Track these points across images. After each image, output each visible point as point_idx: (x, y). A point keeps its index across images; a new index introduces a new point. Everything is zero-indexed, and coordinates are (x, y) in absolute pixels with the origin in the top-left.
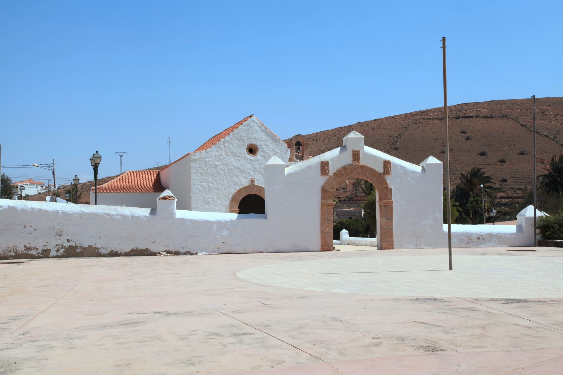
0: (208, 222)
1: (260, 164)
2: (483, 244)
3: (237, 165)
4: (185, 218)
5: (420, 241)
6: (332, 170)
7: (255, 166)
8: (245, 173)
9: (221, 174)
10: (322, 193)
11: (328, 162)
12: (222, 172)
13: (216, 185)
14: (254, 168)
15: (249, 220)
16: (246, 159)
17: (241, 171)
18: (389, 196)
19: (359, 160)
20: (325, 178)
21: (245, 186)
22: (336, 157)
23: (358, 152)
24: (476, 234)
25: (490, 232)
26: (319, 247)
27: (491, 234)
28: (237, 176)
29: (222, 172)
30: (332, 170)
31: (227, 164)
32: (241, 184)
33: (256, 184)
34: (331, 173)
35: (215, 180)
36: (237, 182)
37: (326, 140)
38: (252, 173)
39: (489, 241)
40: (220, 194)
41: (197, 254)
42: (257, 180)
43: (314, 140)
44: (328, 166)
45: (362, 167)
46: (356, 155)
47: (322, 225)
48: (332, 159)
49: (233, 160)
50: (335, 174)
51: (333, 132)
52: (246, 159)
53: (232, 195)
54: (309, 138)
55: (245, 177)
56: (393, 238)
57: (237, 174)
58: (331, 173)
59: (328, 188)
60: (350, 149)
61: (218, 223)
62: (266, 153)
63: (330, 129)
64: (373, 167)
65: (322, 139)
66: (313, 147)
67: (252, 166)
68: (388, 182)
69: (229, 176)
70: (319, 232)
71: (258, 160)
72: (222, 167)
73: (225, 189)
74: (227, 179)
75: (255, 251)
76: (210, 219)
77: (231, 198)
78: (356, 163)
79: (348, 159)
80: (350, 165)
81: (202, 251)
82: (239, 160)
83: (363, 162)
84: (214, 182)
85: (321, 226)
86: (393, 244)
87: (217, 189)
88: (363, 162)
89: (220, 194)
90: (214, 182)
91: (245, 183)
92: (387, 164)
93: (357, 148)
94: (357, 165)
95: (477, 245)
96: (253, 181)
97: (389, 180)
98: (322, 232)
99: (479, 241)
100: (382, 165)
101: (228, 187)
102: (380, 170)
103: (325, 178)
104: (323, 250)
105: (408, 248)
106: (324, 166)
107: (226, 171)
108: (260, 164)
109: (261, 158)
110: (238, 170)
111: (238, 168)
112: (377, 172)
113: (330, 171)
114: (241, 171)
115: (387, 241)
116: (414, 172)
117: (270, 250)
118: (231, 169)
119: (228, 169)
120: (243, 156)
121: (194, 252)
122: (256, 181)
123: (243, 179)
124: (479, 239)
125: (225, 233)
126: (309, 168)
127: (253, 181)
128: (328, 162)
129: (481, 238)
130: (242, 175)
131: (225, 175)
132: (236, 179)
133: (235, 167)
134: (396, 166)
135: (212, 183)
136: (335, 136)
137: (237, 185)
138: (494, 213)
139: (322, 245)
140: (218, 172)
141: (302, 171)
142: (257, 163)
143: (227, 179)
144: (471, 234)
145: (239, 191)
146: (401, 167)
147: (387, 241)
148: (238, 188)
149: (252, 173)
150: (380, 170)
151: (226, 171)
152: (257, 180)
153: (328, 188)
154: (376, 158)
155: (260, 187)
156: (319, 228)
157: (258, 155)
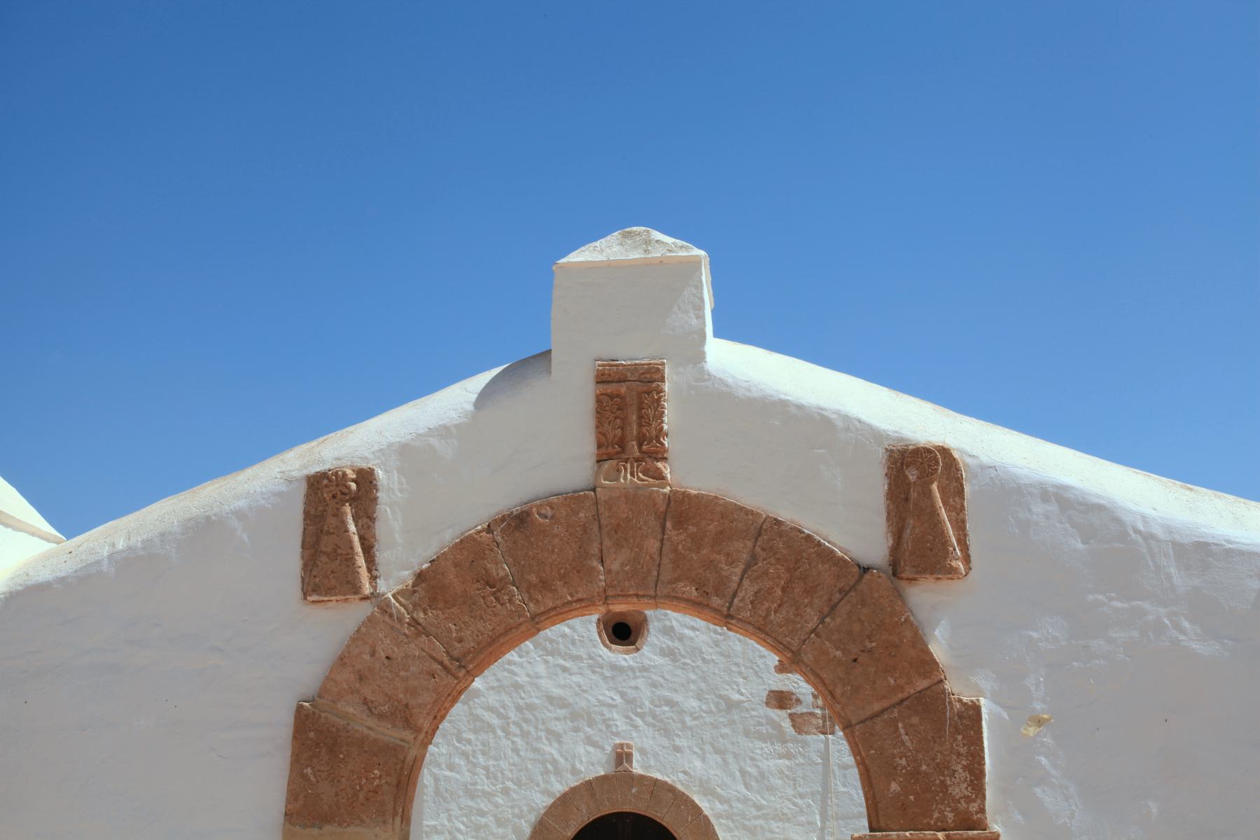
1: (654, 685)
3: (557, 692)
6: (403, 548)
7: (632, 694)
8: (591, 723)
9: (491, 728)
10: (297, 761)
11: (366, 478)
12: (495, 721)
13: (467, 777)
14: (630, 702)
16: (596, 666)
17: (575, 716)
18: (959, 790)
19: (660, 454)
20: (337, 622)
21: (590, 776)
28: (556, 737)
29: (495, 721)
30: (403, 548)
31: (517, 687)
32: (575, 771)
33: (637, 768)
35: (465, 755)
36: (554, 762)
38: (621, 724)
40: (482, 813)
42: (643, 752)
45: (684, 510)
46: (628, 408)
48: (408, 453)
49: (541, 669)
50: (428, 584)
52: (596, 666)
53: (533, 818)
55: (589, 741)
57: (558, 727)
58: (394, 572)
59: (350, 708)
60: (582, 347)
62: (681, 638)
64: (786, 515)
67: (623, 695)
68: (939, 649)
69: (525, 735)
71: (644, 669)
72: (492, 699)
73: (506, 791)
74: (516, 750)
78: (628, 479)
79: (555, 448)
80: (573, 499)
82: (565, 669)
84: (458, 760)
87: (471, 795)
88: (690, 467)
89: (482, 813)
90: (458, 760)
91: (592, 763)
92: (918, 476)
94: (632, 498)
96: (622, 756)
97: (951, 627)
100: (874, 488)
101: (518, 783)
102: (854, 527)
103: (337, 622)
106: (336, 511)
107: (513, 715)
108: (654, 685)
109: (659, 660)
110: (561, 712)
111: (561, 703)
112: (826, 555)
113: (382, 556)
114: (575, 716)
118: (530, 707)
119: (519, 708)
120: (582, 652)
122: (636, 756)
123: (581, 749)
127: (622, 756)
128: (366, 478)
130: (576, 730)
131: (508, 734)
132: (551, 750)
133: (551, 699)
134: (1013, 492)
135: (451, 767)
137: (558, 772)
138: (363, 630)
140: (477, 718)
142: (640, 682)
143: (516, 750)
145: (565, 802)
146: (1062, 499)
148: (559, 788)
149: (621, 724)
150: (854, 527)
151: (513, 715)
152: (643, 752)
153: (352, 715)
154: (817, 427)
155: (656, 782)
157: (645, 649)
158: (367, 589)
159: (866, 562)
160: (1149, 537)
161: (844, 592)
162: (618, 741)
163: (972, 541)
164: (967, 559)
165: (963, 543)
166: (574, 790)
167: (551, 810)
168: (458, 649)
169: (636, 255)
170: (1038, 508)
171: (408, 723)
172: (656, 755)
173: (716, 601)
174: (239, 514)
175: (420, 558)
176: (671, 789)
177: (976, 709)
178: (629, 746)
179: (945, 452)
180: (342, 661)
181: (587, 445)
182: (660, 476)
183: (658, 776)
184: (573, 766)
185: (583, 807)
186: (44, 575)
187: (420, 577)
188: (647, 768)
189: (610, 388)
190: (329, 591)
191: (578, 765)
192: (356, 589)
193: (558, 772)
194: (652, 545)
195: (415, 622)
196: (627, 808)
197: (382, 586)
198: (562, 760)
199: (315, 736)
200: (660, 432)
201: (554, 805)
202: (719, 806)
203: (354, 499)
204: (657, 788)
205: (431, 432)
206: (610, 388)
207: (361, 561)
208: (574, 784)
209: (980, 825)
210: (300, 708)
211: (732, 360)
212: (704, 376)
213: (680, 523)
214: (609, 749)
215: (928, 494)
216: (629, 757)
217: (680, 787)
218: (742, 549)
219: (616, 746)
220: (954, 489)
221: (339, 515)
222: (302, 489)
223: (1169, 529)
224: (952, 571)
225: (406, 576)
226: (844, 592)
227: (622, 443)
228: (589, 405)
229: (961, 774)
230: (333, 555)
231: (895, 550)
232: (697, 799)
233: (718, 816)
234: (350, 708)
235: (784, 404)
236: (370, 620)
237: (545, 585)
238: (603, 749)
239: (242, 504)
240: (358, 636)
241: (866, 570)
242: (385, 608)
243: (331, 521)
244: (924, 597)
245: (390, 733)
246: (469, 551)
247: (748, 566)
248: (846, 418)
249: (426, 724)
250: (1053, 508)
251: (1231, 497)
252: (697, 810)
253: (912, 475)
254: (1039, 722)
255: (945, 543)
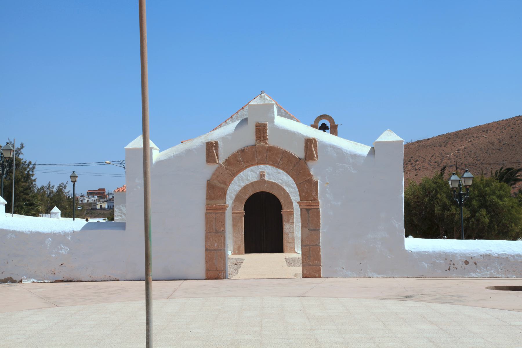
0: (38, 234)
2: (475, 272)
4: (5, 228)
5: (363, 264)
6: (223, 155)
10: (208, 190)
11: (216, 143)
15: (99, 230)
18: (314, 194)
20: (213, 167)
21: (252, 181)
22: (229, 135)
23: (265, 126)
24: (462, 255)
25: (488, 253)
26: (203, 274)
27: (490, 256)
30: (223, 155)
32: (248, 180)
33: (267, 179)
34: (222, 158)
37: (498, 131)
39: (486, 267)
41: (21, 281)
42: (268, 174)
43: (483, 131)
44: (217, 150)
45: (270, 149)
46: (261, 131)
47: (207, 239)
48: (223, 139)
51: (507, 122)
53: (235, 193)
54: (478, 129)
56: (320, 260)
58: (222, 158)
59: (216, 182)
61: (54, 236)
63: (505, 119)
64: (288, 150)
65: (494, 130)
66: (481, 138)
68: (312, 173)
70: (203, 249)
75: (66, 279)
76: (41, 230)
77: (234, 197)
78: (261, 143)
79: (249, 138)
80: (252, 147)
81: (30, 277)
83: (272, 141)
85: (206, 241)
86: (320, 270)
88: (272, 141)
92: (310, 144)
93: (262, 121)
94: (262, 147)
95: (463, 274)
98: (207, 250)
99: (468, 266)
100: (303, 145)
102: (299, 152)
103: (213, 167)
104: (208, 278)
105: (345, 276)
113: (220, 156)
115: (310, 265)
116: (355, 156)
117: (129, 277)
121: (18, 280)
122: (266, 175)
124: (467, 263)
125: (64, 251)
126: (189, 152)
128: (216, 143)
129: (471, 262)
134: (325, 146)
136: (510, 126)
137: (243, 180)
139: (207, 270)
141: (178, 158)
144: (454, 255)
145: (245, 188)
147: (310, 265)
150: (299, 152)
152: (268, 174)
155: (272, 183)
156: (204, 243)
158: (217, 162)
159: (301, 158)
160: (347, 154)
161: (297, 163)
162: (261, 171)
163: (318, 154)
164: (317, 157)
165: (317, 155)
166: (247, 185)
167: (241, 191)
168: (233, 172)
169: (262, 103)
170: (329, 149)
171: (225, 184)
172: (272, 175)
173: (276, 164)
174: (195, 149)
175: (226, 157)
176: (277, 185)
177: (317, 182)
178: (264, 172)
179: (314, 139)
180: (214, 174)
181: (254, 137)
182: (266, 143)
183: (273, 181)
184: (247, 178)
185: (251, 190)
186: (162, 159)
187: (226, 160)
188: (270, 178)
189: (258, 127)
190: (211, 162)
191: (249, 178)
192: (216, 162)
193: (243, 180)
194: (265, 155)
195: (226, 168)
196: (264, 190)
197: (220, 162)
198: (243, 176)
199: (210, 186)
200: (267, 135)
201: (241, 190)
202: (291, 190)
203: (215, 147)
204: (272, 184)
205: (227, 135)
206: (258, 127)
207: (216, 157)
208: (247, 183)
209: (317, 200)
210: (207, 182)
211: (280, 121)
212: (274, 125)
213: (270, 151)
214: (258, 173)
215: (311, 147)
216: (264, 175)
217: (279, 184)
218: (280, 156)
219: (260, 172)
220: (316, 146)
221: (212, 150)
222: (205, 144)
223: (350, 152)
224: (315, 160)
225: (224, 160)
226: (297, 163)
227: (260, 137)
228: (254, 130)
229: (314, 192)
230: (212, 156)
231: (306, 156)
232: (285, 188)
233: (291, 193)
234: (216, 182)
235: (288, 130)
236: (218, 167)
237: (247, 162)
238: (256, 173)
239: (195, 147)
240: (216, 170)
241: (301, 159)
242: (221, 165)
243: (211, 151)
244: (310, 164)
245: (223, 186)
246: (234, 156)
247: (281, 159)
248: (298, 133)
249: (228, 184)
250: (332, 149)
251: (363, 145)
252: (285, 191)
253: (309, 143)
254: (327, 184)
255: (314, 155)
